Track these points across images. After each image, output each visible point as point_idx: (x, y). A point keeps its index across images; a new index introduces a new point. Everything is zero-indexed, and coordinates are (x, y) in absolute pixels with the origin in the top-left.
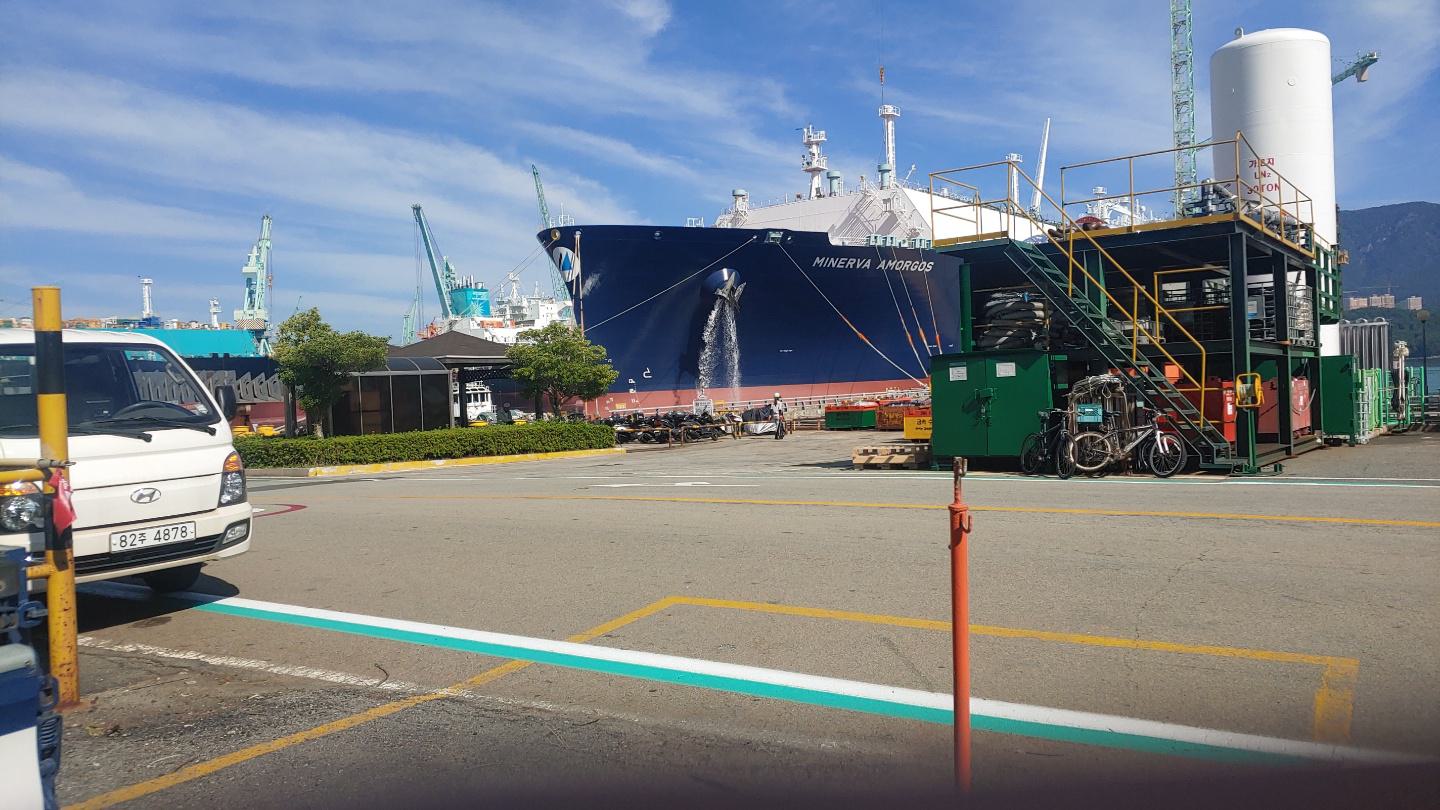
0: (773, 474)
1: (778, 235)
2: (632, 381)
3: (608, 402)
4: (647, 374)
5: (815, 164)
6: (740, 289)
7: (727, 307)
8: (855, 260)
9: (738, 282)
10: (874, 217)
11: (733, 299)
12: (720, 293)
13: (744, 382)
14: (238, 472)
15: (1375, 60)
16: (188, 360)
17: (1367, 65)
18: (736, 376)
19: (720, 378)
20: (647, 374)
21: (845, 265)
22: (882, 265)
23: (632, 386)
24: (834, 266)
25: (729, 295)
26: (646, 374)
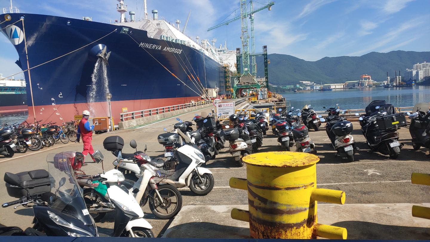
0: (376, 172)
1: (127, 30)
2: (53, 99)
3: (41, 110)
4: (60, 96)
5: (122, 8)
6: (109, 54)
7: (103, 63)
8: (155, 45)
9: (108, 51)
10: (152, 31)
11: (106, 59)
12: (100, 55)
13: (112, 99)
14: (174, 130)
15: (274, 4)
16: (97, 226)
17: (271, 6)
18: (109, 96)
19: (100, 97)
20: (60, 96)
21: (151, 47)
22: (165, 49)
23: (53, 102)
24: (147, 44)
25: (104, 57)
26: (60, 96)
